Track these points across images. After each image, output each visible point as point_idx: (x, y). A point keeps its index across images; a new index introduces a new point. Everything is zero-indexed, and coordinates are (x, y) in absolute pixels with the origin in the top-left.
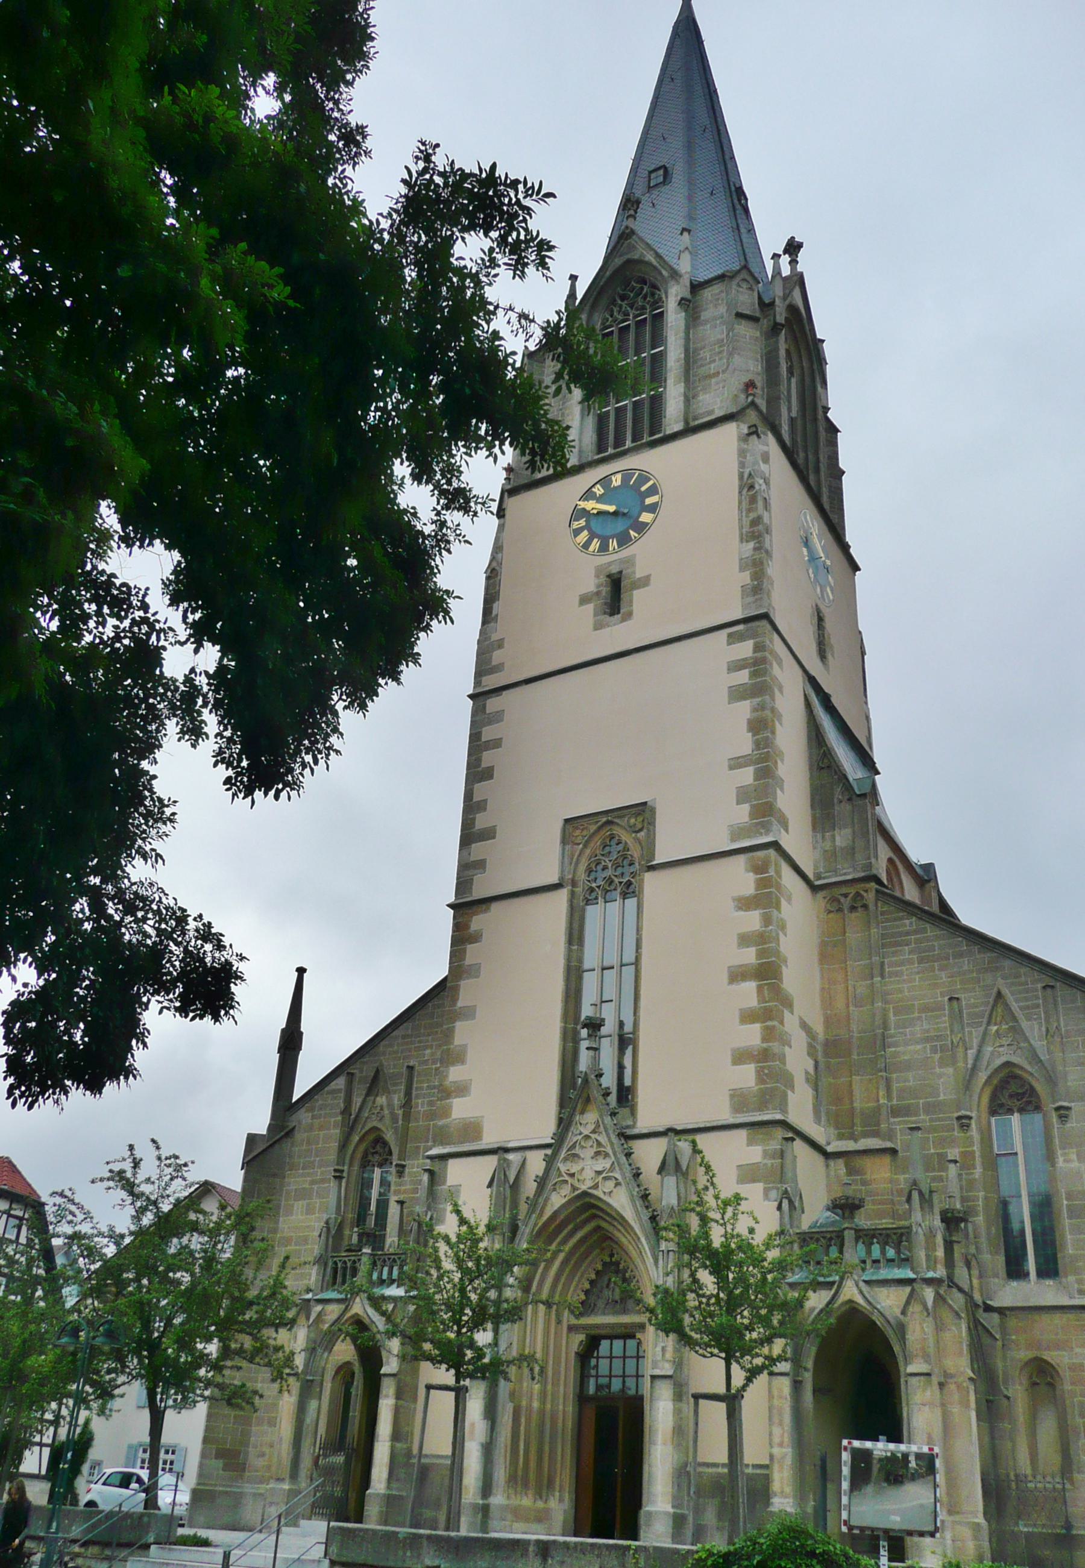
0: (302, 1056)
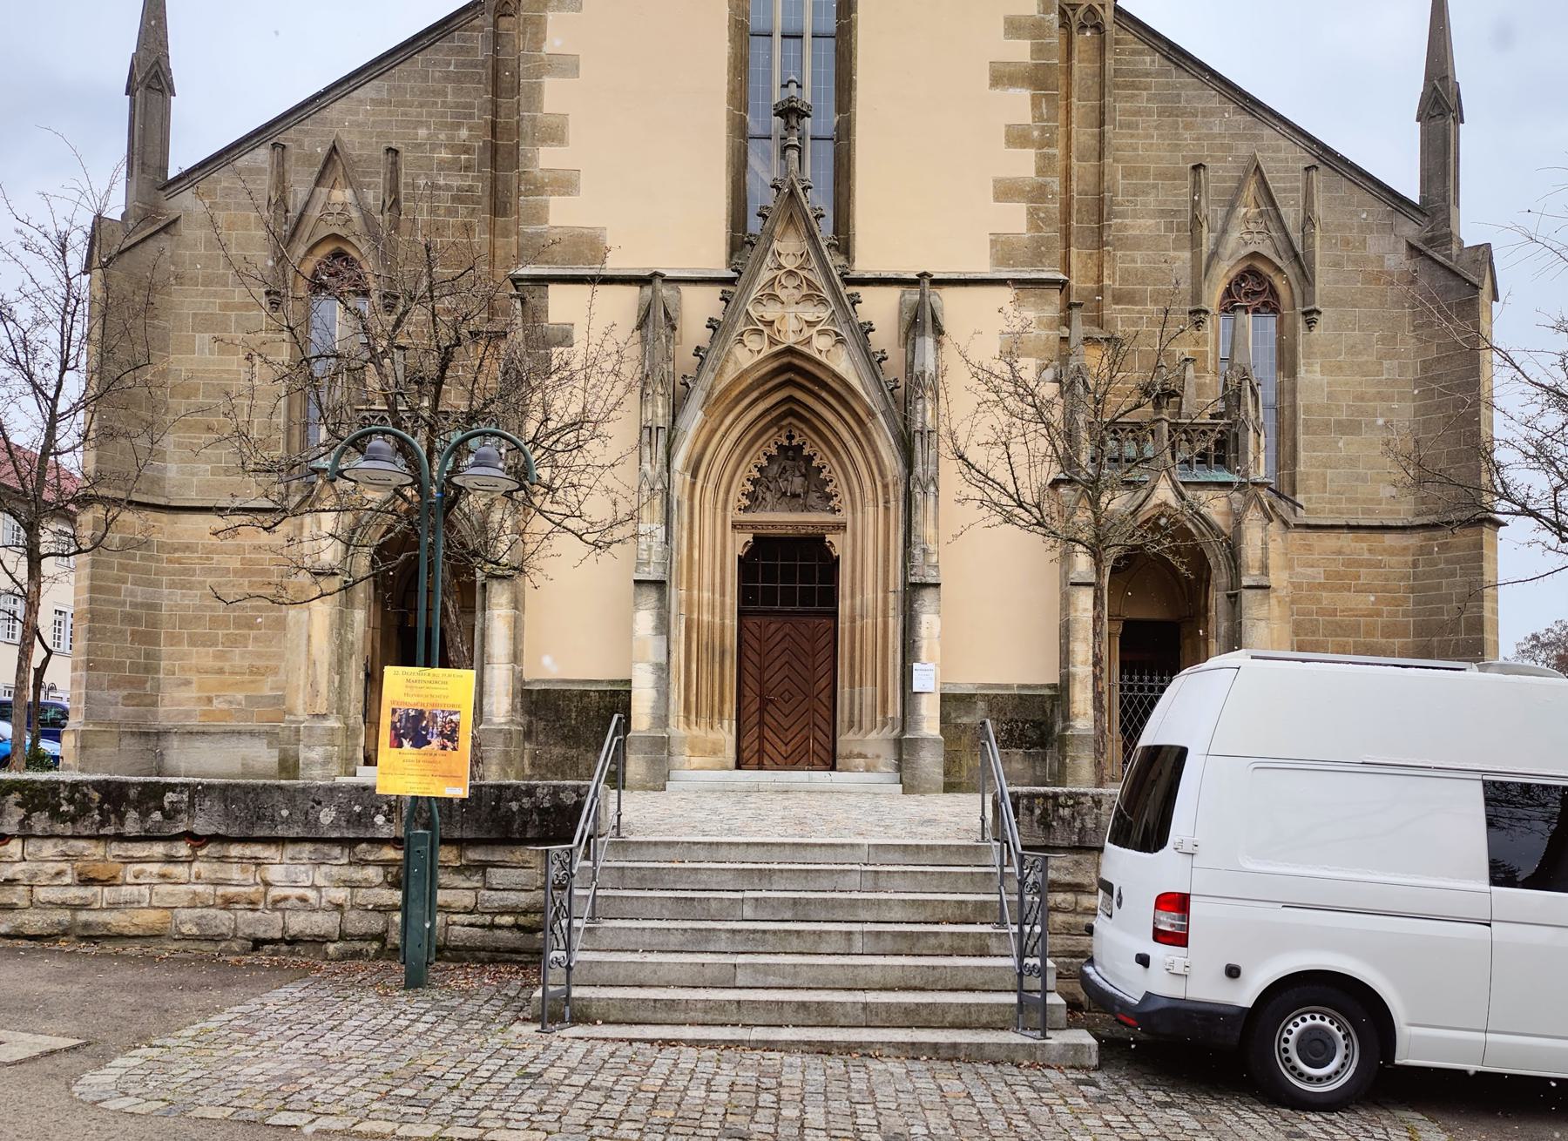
0: (178, 105)
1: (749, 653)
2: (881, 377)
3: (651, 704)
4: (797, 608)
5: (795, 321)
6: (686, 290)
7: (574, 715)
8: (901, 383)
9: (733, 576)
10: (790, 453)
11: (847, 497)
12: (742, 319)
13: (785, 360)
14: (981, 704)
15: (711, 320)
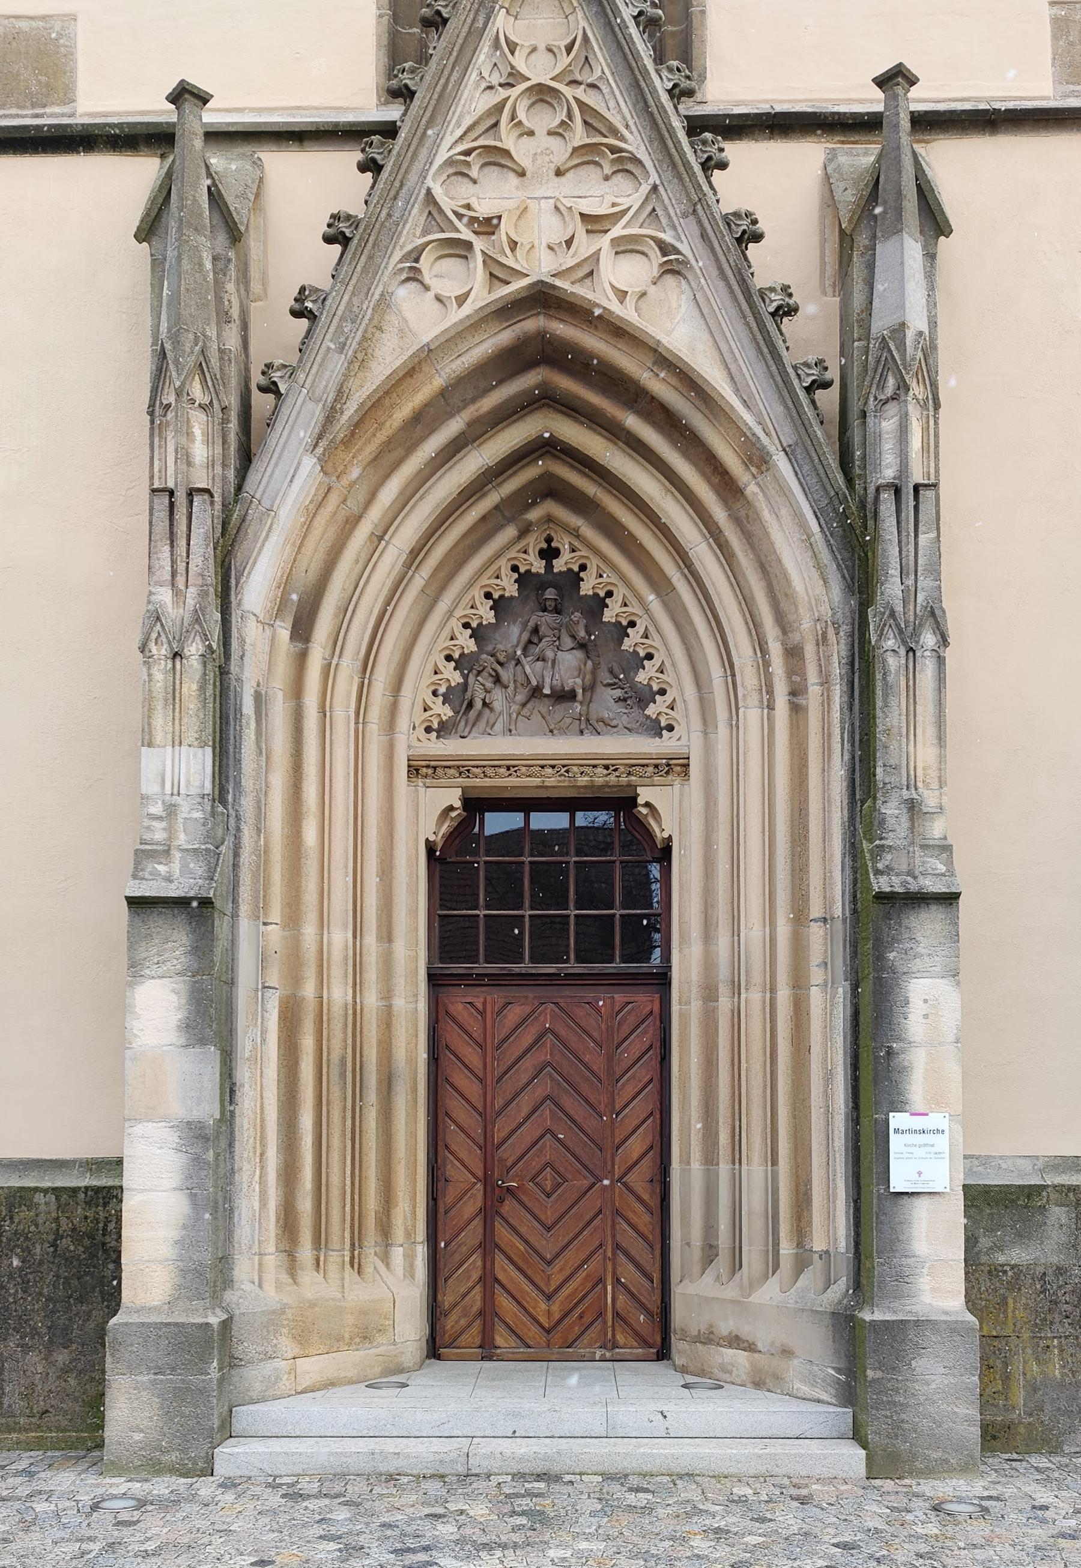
1: (461, 1079)
2: (784, 353)
3: (175, 1234)
4: (573, 966)
5: (554, 220)
10: (550, 594)
11: (690, 691)
12: (417, 215)
13: (531, 324)
14: (1058, 1214)
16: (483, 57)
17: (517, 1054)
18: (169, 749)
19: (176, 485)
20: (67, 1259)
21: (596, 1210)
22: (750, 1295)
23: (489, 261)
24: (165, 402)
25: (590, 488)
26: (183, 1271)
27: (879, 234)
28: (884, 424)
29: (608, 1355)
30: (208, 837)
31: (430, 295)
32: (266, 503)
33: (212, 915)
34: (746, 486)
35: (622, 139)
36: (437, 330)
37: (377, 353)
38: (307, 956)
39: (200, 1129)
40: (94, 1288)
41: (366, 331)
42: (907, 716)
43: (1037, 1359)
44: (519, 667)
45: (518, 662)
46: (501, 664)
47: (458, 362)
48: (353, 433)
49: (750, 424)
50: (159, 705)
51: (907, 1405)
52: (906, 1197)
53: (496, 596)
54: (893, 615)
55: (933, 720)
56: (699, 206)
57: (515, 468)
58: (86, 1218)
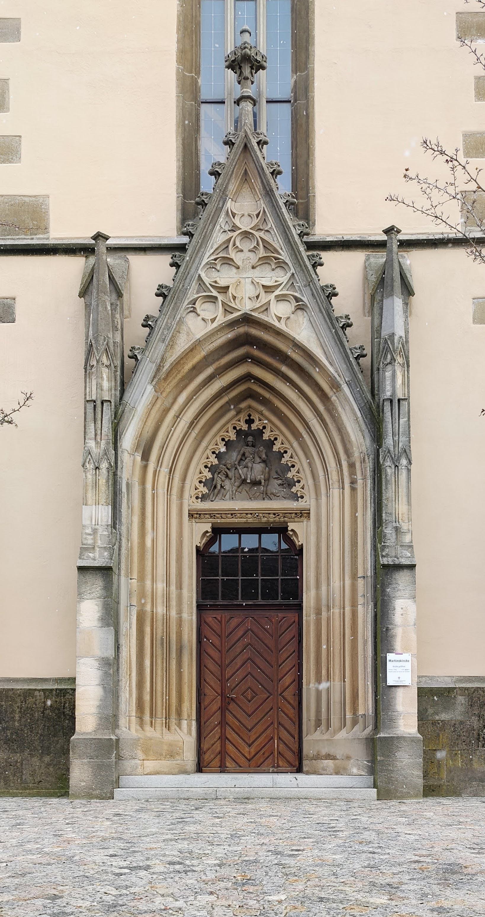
1: (211, 651)
2: (346, 343)
3: (97, 703)
5: (252, 287)
6: (135, 260)
7: (17, 717)
8: (368, 351)
9: (191, 569)
10: (250, 439)
11: (310, 482)
12: (194, 285)
13: (242, 330)
14: (461, 699)
15: (161, 286)
16: (222, 219)
17: (237, 638)
18: (94, 506)
19: (97, 398)
20: (48, 719)
21: (270, 707)
22: (334, 736)
23: (224, 304)
24: (91, 364)
25: (267, 395)
26: (101, 718)
27: (385, 296)
28: (386, 374)
29: (275, 770)
30: (110, 542)
31: (200, 318)
32: (132, 405)
33: (112, 573)
34: (331, 397)
35: (281, 255)
36: (203, 333)
37: (178, 342)
38: (147, 593)
39: (108, 660)
40: (59, 731)
41: (173, 333)
42: (395, 493)
43: (452, 759)
44: (236, 471)
45: (236, 468)
46: (228, 469)
47: (211, 345)
48: (167, 375)
49: (333, 372)
50: (90, 488)
51: (394, 771)
52: (394, 688)
53: (226, 440)
54: (389, 452)
55: (406, 494)
56: (311, 283)
57: (235, 386)
58: (56, 701)
